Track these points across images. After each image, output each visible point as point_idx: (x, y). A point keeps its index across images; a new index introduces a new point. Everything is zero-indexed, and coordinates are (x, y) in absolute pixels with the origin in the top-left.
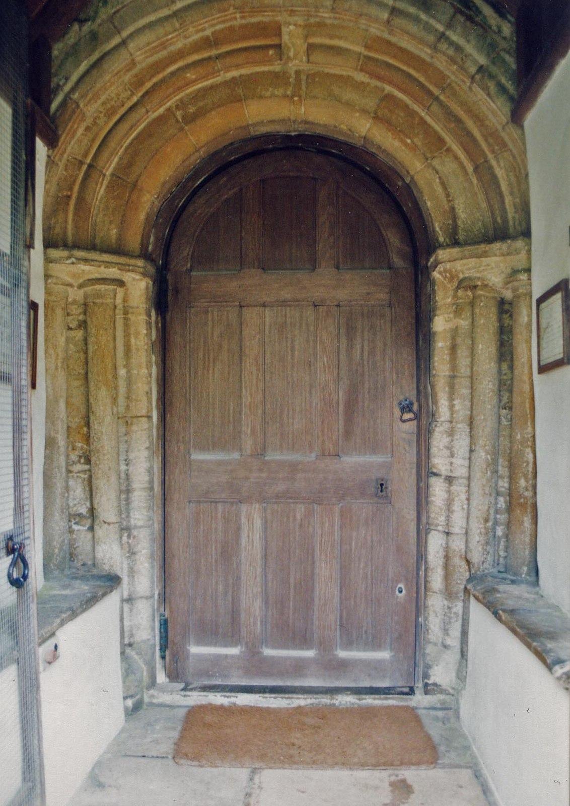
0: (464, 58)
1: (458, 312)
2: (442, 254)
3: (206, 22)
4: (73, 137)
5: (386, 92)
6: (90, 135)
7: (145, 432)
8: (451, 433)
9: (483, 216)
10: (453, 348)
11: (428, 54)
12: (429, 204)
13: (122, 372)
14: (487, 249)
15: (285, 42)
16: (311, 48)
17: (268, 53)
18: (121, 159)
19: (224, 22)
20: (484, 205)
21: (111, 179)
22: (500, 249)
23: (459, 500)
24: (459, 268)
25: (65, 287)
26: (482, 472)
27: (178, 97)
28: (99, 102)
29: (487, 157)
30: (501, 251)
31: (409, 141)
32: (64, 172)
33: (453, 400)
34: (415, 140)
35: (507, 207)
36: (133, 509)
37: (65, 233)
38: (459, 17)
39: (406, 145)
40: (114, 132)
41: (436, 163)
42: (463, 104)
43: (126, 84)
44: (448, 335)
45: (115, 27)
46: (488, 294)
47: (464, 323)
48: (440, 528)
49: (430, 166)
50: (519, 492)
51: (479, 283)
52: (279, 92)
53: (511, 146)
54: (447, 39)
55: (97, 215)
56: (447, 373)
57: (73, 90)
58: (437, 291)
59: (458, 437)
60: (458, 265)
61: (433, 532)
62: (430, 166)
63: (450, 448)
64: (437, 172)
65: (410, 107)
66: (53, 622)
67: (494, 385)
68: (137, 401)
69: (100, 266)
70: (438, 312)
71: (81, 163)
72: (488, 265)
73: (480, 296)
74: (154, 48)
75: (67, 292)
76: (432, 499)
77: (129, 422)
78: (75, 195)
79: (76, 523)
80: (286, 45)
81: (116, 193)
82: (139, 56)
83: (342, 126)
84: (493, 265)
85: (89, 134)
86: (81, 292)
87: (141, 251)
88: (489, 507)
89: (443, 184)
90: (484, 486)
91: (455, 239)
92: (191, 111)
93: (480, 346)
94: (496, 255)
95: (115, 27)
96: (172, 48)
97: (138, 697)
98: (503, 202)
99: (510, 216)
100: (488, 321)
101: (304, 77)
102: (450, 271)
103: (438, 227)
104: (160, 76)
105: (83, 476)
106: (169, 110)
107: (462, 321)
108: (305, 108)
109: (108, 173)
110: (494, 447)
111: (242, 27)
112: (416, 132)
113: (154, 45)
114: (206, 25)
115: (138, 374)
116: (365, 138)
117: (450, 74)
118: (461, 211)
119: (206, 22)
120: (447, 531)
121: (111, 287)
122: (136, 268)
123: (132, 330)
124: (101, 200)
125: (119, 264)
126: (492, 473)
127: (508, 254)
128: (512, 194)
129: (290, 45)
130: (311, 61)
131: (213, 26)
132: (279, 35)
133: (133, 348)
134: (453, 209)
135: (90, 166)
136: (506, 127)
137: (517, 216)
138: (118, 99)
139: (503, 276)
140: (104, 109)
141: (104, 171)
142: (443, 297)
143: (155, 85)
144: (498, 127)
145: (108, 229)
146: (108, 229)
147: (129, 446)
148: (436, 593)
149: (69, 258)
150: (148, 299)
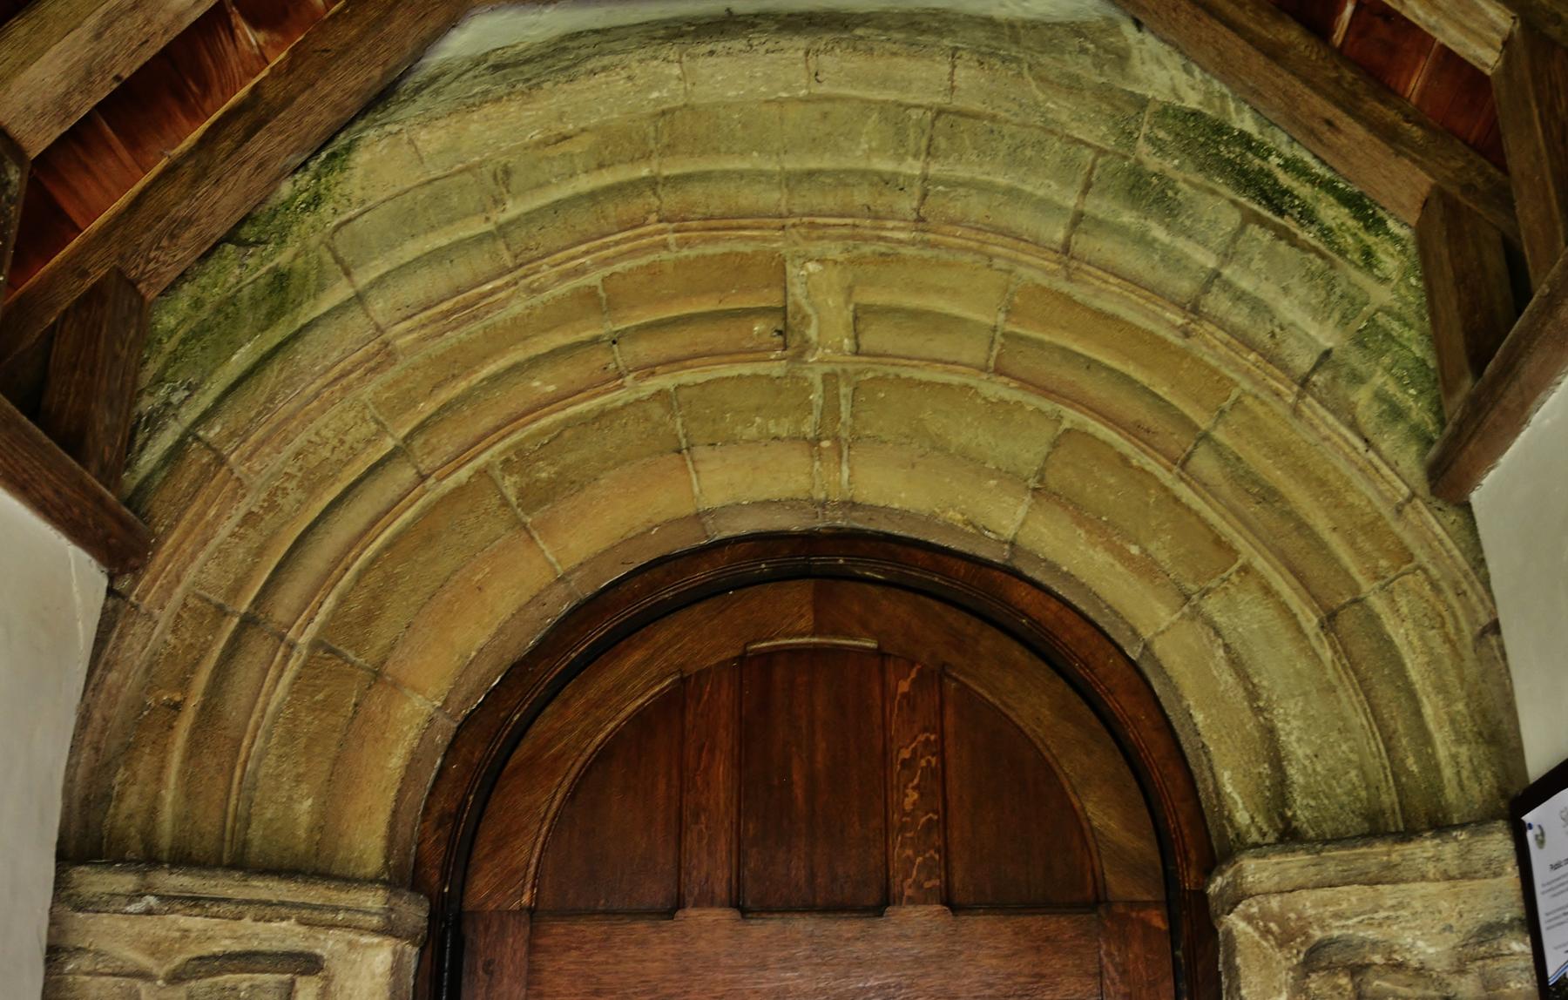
0: (1277, 330)
2: (1255, 871)
3: (587, 253)
5: (1066, 425)
6: (254, 538)
12: (1199, 718)
14: (1395, 857)
15: (795, 303)
16: (862, 316)
17: (751, 329)
18: (343, 601)
19: (632, 253)
20: (1360, 720)
21: (310, 657)
24: (1311, 912)
25: (124, 982)
27: (508, 442)
28: (288, 450)
30: (1441, 865)
31: (1134, 550)
32: (169, 637)
34: (1152, 547)
35: (1432, 726)
37: (153, 812)
38: (1254, 229)
39: (1127, 559)
40: (322, 527)
41: (1211, 605)
52: (784, 428)
53: (1422, 556)
54: (1228, 286)
55: (264, 753)
57: (206, 417)
58: (1243, 971)
60: (1307, 903)
62: (1197, 614)
64: (1218, 633)
66: (1160, 176)
71: (221, 612)
72: (1401, 905)
80: (799, 308)
81: (320, 697)
82: (403, 336)
83: (951, 513)
85: (251, 533)
87: (387, 859)
89: (1236, 664)
91: (1282, 816)
92: (544, 475)
94: (1424, 878)
98: (1418, 713)
99: (1442, 753)
101: (844, 390)
102: (1282, 920)
103: (1235, 789)
104: (462, 385)
106: (482, 472)
108: (851, 468)
109: (304, 640)
111: (679, 264)
112: (1153, 523)
114: (587, 260)
116: (1012, 544)
117: (1236, 377)
118: (1293, 738)
119: (587, 253)
122: (359, 916)
124: (276, 716)
125: (304, 906)
127: (1464, 876)
128: (1442, 689)
129: (810, 311)
130: (864, 347)
131: (606, 262)
134: (1270, 732)
135: (248, 621)
136: (1408, 508)
137: (1464, 752)
139: (1454, 939)
140: (300, 469)
143: (446, 407)
144: (1382, 511)
145: (290, 798)
146: (290, 798)
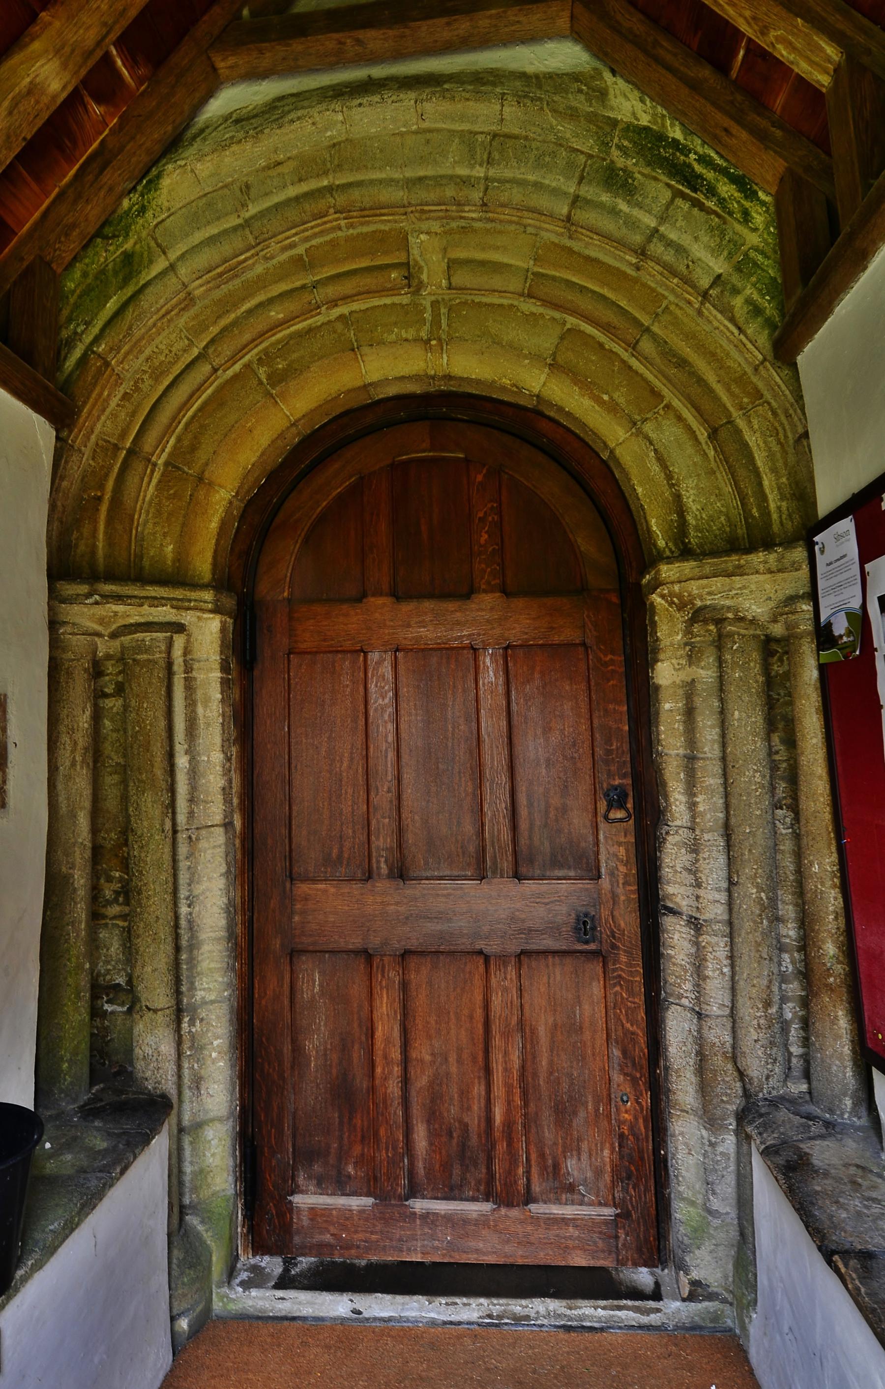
1: (693, 656)
3: (296, 234)
4: (104, 410)
5: (568, 326)
6: (130, 407)
7: (219, 850)
8: (694, 848)
9: (727, 507)
10: (689, 713)
11: (631, 264)
12: (639, 490)
13: (182, 761)
14: (742, 562)
16: (453, 265)
18: (179, 440)
22: (766, 562)
23: (715, 958)
26: (755, 922)
27: (260, 348)
28: (142, 357)
29: (731, 416)
30: (767, 566)
31: (606, 397)
32: (91, 462)
33: (695, 795)
34: (616, 396)
36: (199, 974)
37: (93, 552)
38: (679, 202)
41: (648, 428)
42: (690, 336)
43: (181, 331)
44: (681, 692)
45: (159, 245)
46: (743, 631)
47: (706, 674)
48: (685, 1002)
49: (639, 432)
50: (824, 964)
51: (730, 615)
52: (410, 334)
53: (768, 396)
54: (662, 237)
55: (146, 522)
56: (681, 751)
57: (97, 340)
59: (706, 855)
60: (694, 587)
61: (673, 1008)
63: (693, 871)
64: (651, 443)
65: (607, 347)
67: (764, 777)
68: (206, 802)
69: (141, 605)
70: (662, 656)
71: (116, 448)
72: (744, 587)
73: (731, 635)
74: (220, 275)
75: (96, 644)
76: (669, 952)
77: (194, 837)
78: (107, 496)
79: (109, 1002)
81: (172, 492)
84: (753, 587)
86: (117, 643)
88: (770, 981)
90: (758, 944)
91: (683, 543)
93: (736, 713)
94: (757, 572)
95: (159, 245)
96: (250, 275)
97: (199, 1309)
98: (760, 484)
99: (772, 506)
100: (746, 673)
102: (680, 596)
103: (657, 527)
105: (121, 923)
106: (247, 366)
107: (701, 671)
109: (160, 462)
110: (770, 878)
113: (219, 270)
114: (296, 239)
115: (208, 761)
117: (666, 293)
119: (296, 234)
120: (697, 1009)
121: (160, 635)
123: (199, 694)
126: (771, 922)
127: (779, 571)
128: (774, 470)
129: (422, 263)
131: (307, 239)
132: (405, 245)
133: (201, 722)
134: (678, 497)
135: (131, 452)
136: (761, 368)
138: (170, 351)
141: (154, 459)
142: (669, 632)
143: (225, 329)
147: (193, 874)
148: (687, 1112)
149: (89, 595)
150: (223, 646)
